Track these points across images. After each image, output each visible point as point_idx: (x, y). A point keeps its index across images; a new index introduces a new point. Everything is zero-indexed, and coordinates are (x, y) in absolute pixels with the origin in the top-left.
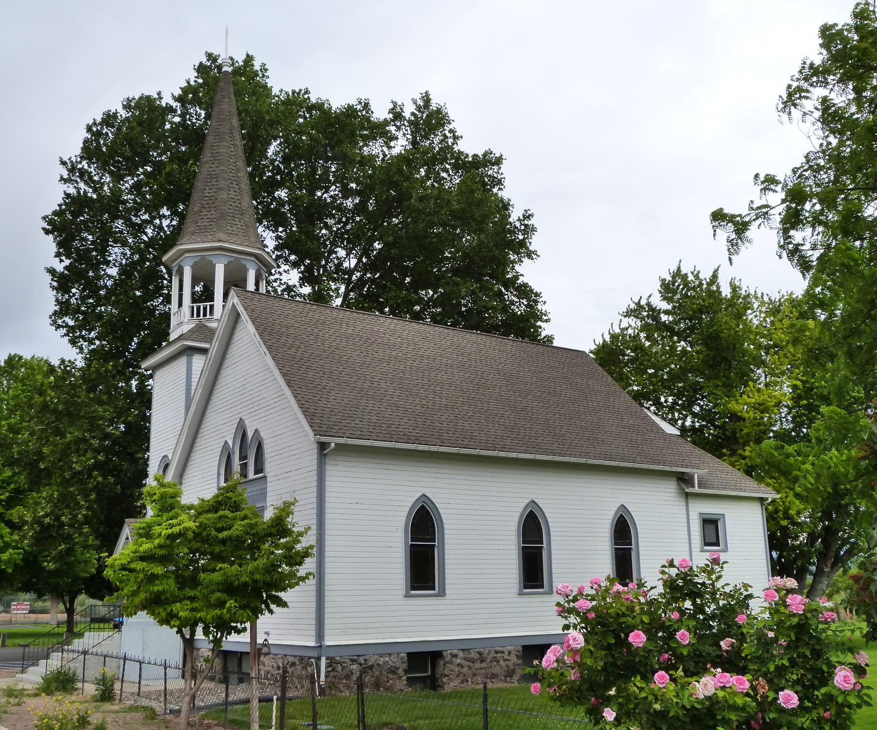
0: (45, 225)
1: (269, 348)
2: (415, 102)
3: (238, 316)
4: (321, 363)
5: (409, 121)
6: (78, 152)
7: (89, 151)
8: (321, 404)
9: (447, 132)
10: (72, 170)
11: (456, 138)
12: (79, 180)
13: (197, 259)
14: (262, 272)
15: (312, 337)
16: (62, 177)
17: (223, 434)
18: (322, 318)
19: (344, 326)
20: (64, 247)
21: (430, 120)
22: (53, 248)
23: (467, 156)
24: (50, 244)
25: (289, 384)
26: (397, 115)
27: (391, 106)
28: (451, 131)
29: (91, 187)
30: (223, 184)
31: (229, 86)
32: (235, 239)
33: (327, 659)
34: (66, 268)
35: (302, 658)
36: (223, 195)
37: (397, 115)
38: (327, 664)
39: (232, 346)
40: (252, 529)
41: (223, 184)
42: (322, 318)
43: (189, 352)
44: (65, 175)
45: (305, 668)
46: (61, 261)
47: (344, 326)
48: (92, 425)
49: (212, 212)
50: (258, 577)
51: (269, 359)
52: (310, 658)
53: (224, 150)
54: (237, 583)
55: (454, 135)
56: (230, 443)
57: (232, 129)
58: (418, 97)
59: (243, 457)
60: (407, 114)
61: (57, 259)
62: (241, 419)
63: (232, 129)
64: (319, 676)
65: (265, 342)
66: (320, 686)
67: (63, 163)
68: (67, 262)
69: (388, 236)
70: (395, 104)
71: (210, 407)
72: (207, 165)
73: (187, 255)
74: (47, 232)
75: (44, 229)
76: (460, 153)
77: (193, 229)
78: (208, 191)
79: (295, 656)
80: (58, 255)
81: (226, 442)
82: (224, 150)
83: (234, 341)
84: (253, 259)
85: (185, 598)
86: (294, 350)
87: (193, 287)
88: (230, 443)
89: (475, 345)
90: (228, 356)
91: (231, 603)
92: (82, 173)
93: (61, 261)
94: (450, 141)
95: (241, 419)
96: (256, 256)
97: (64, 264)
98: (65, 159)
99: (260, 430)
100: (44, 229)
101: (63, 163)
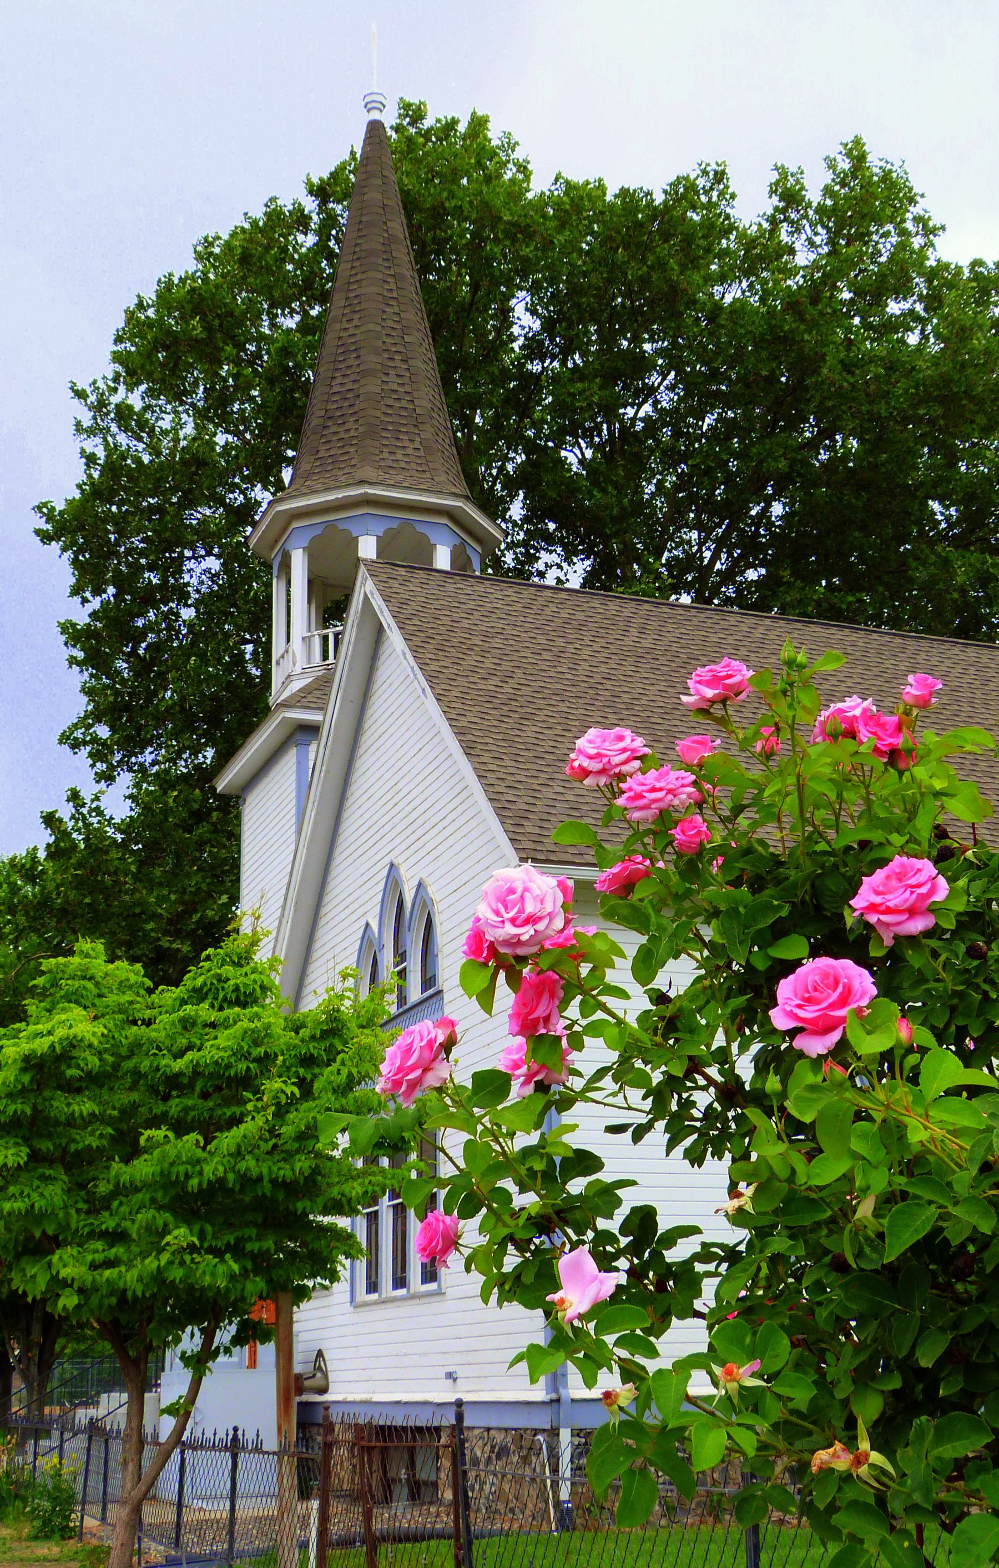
0: (43, 525)
1: (431, 679)
2: (831, 164)
3: (380, 630)
4: (563, 707)
5: (821, 210)
6: (110, 369)
7: (132, 369)
8: (548, 793)
9: (909, 225)
10: (100, 406)
11: (929, 231)
12: (114, 428)
13: (318, 531)
14: (469, 552)
15: (546, 655)
16: (78, 424)
17: (359, 913)
18: (580, 616)
19: (634, 632)
20: (88, 577)
21: (867, 198)
22: (69, 577)
23: (959, 269)
24: (57, 565)
25: (469, 750)
26: (789, 195)
27: (775, 176)
28: (917, 219)
29: (140, 439)
30: (372, 360)
31: (430, 202)
32: (400, 478)
33: (576, 1433)
34: (94, 615)
35: (520, 1434)
36: (372, 386)
37: (789, 195)
38: (576, 1447)
39: (373, 699)
40: (256, 1043)
41: (372, 360)
42: (580, 616)
43: (299, 737)
44: (87, 419)
45: (525, 1460)
46: (85, 601)
47: (634, 632)
48: (133, 934)
49: (347, 426)
50: (249, 1164)
51: (431, 703)
52: (536, 1432)
53: (374, 289)
54: (194, 1182)
55: (925, 226)
56: (374, 926)
57: (389, 241)
58: (835, 151)
59: (401, 956)
60: (814, 195)
61: (77, 599)
62: (392, 865)
63: (389, 241)
64: (555, 1484)
65: (423, 666)
66: (558, 1504)
67: (80, 394)
68: (95, 604)
69: (776, 459)
70: (783, 173)
71: (337, 851)
72: (338, 326)
73: (295, 525)
74: (45, 537)
75: (38, 532)
76: (943, 266)
77: (308, 467)
78: (339, 380)
79: (506, 1430)
80: (76, 591)
81: (367, 925)
82: (374, 289)
83: (375, 687)
84: (444, 521)
85: (92, 1235)
86: (495, 681)
87: (344, 630)
88: (374, 926)
89: (972, 670)
90: (366, 726)
91: (181, 1235)
92: (123, 413)
93: (85, 601)
94: (917, 242)
95: (392, 865)
96: (451, 515)
97: (90, 608)
98: (83, 385)
99: (428, 881)
100: (38, 532)
101: (80, 394)
